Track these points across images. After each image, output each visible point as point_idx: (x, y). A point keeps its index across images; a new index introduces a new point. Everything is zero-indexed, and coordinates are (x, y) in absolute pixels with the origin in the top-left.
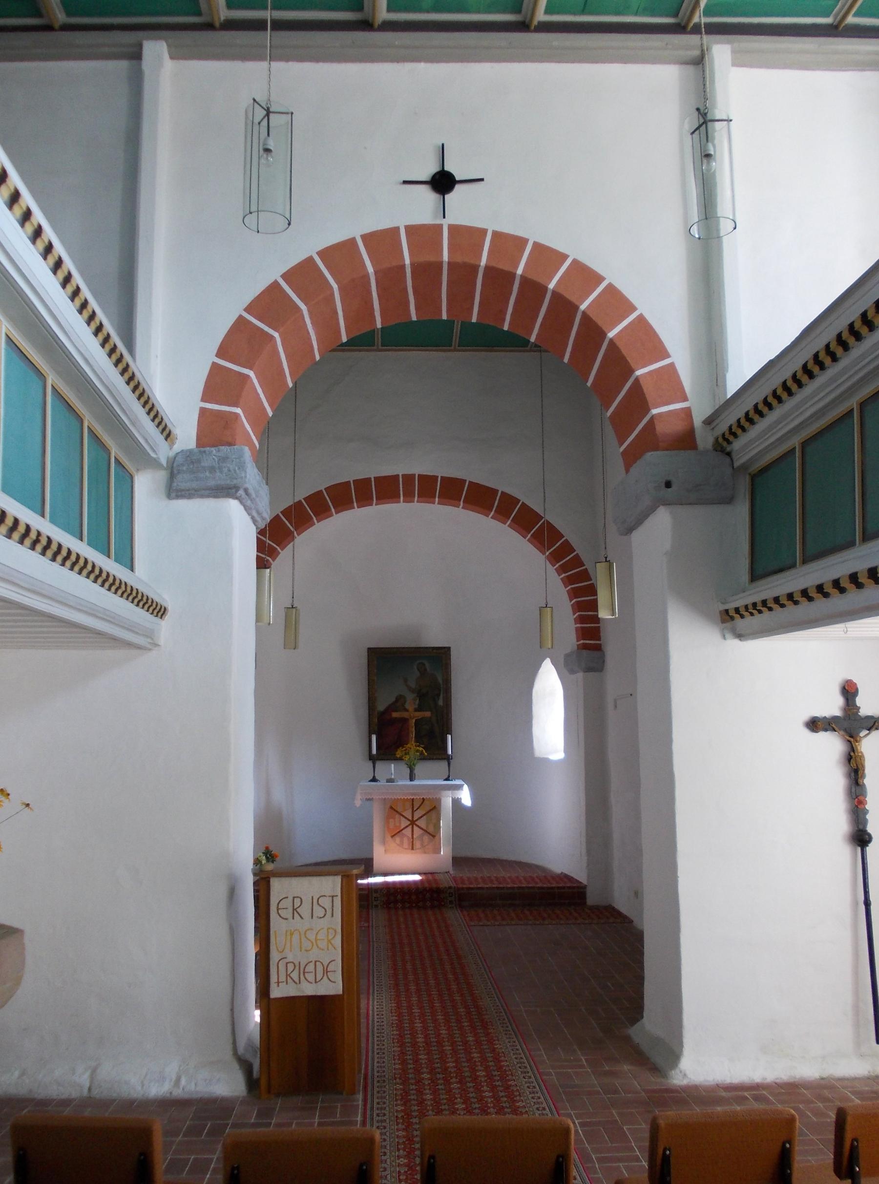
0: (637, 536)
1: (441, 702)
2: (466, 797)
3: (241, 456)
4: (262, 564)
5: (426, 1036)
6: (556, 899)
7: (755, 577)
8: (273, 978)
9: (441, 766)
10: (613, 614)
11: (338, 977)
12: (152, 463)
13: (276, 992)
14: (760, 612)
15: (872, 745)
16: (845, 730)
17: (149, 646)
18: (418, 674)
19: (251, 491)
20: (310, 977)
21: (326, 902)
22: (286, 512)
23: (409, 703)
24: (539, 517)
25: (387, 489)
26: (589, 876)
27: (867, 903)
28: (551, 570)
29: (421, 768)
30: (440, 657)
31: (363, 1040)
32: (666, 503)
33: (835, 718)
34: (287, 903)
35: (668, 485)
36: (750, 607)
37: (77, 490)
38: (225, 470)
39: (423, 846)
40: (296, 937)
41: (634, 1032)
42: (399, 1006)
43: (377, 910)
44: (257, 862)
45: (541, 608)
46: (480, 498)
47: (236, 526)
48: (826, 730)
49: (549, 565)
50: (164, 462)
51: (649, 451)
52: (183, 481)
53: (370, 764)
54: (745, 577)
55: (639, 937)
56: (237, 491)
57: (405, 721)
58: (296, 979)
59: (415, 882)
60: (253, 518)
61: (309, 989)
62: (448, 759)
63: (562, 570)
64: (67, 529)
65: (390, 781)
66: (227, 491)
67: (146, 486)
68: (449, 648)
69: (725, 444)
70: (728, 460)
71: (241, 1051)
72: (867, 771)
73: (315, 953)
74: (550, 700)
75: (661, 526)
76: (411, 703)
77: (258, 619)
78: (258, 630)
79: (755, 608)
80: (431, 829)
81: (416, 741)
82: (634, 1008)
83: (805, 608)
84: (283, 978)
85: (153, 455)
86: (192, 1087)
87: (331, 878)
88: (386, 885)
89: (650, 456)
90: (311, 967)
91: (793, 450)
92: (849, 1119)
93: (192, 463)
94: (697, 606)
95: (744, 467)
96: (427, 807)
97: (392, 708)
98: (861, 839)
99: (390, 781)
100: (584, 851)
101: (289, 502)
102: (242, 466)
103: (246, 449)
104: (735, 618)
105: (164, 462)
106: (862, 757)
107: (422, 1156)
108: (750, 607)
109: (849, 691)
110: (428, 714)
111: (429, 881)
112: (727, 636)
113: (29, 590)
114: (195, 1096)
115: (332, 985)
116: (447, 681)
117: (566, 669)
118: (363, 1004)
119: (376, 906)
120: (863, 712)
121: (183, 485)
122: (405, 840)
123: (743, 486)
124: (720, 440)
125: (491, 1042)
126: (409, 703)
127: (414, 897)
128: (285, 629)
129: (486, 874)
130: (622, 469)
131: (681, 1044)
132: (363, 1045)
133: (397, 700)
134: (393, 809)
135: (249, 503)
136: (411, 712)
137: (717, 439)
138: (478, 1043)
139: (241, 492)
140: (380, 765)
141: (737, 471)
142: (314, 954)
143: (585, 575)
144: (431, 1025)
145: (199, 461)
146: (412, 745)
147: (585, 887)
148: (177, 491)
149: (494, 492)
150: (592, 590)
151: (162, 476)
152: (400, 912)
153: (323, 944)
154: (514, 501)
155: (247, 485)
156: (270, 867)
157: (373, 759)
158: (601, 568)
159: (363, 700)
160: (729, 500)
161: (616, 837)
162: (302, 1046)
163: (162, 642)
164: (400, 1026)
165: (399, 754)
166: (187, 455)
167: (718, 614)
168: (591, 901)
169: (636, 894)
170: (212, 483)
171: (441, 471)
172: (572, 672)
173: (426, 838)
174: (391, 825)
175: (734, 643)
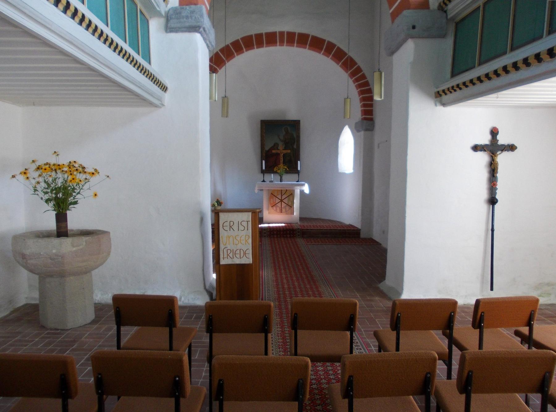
0: (396, 56)
1: (295, 147)
2: (306, 189)
3: (201, 10)
4: (213, 70)
5: (288, 285)
6: (347, 235)
7: (454, 74)
8: (221, 256)
9: (295, 176)
10: (381, 97)
11: (250, 256)
12: (158, 14)
13: (223, 262)
14: (455, 91)
15: (502, 158)
16: (490, 151)
17: (160, 105)
18: (284, 133)
19: (206, 29)
20: (238, 256)
21: (245, 224)
22: (222, 50)
23: (280, 146)
24: (345, 54)
25: (271, 39)
26: (362, 226)
27: (493, 230)
28: (351, 81)
29: (285, 177)
30: (295, 125)
31: (261, 286)
32: (412, 37)
33: (486, 145)
34: (227, 224)
35: (414, 27)
36: (450, 88)
37: (123, 22)
38: (194, 18)
39: (286, 211)
40: (231, 239)
41: (381, 286)
42: (276, 274)
43: (266, 237)
44: (213, 205)
45: (345, 99)
46: (317, 44)
47: (198, 48)
48: (481, 151)
49: (350, 79)
50: (163, 13)
51: (405, 9)
52: (172, 24)
53: (262, 175)
54: (449, 75)
55: (385, 251)
56: (200, 29)
57: (278, 154)
58: (232, 257)
59: (282, 226)
60: (207, 45)
61: (237, 261)
62: (298, 172)
63: (356, 81)
64: (119, 36)
65: (271, 181)
66: (194, 29)
67: (155, 26)
68: (299, 121)
69: (444, 6)
70: (445, 15)
71: (207, 287)
72: (499, 170)
73: (239, 247)
74: (347, 142)
75: (409, 47)
76: (281, 147)
77: (211, 98)
78: (211, 103)
79: (453, 89)
80: (290, 204)
81: (283, 164)
82: (382, 276)
83: (479, 87)
84: (225, 256)
85: (158, 9)
86: (186, 301)
87: (246, 213)
88: (269, 227)
89: (406, 12)
90: (238, 252)
91: (479, 7)
92: (481, 303)
93: (177, 14)
94: (424, 89)
95: (453, 19)
96: (288, 194)
97: (272, 148)
98: (492, 201)
99: (271, 181)
100: (360, 214)
101: (222, 45)
102: (202, 16)
103: (204, 7)
104: (442, 96)
105: (163, 13)
106: (497, 164)
107: (291, 314)
108: (450, 88)
109: (494, 133)
110: (289, 151)
111: (288, 226)
112: (438, 104)
113: (104, 64)
114: (188, 305)
115: (248, 260)
116: (298, 137)
117: (356, 130)
118: (261, 272)
119: (265, 236)
120: (500, 143)
121: (173, 26)
122: (278, 208)
123: (452, 29)
124: (442, 4)
125: (317, 288)
126: (280, 146)
127: (282, 233)
128: (222, 106)
129: (315, 224)
130: (390, 21)
131: (402, 289)
132: (261, 288)
133: (274, 145)
134: (272, 194)
135: (205, 36)
136: (281, 150)
137: (440, 4)
138: (311, 288)
139: (201, 29)
140: (266, 175)
141: (448, 21)
142: (239, 246)
143: (367, 84)
144: (290, 281)
145: (180, 13)
146: (281, 165)
147: (360, 230)
148: (170, 29)
149: (324, 41)
150: (370, 91)
151: (162, 21)
152: (276, 239)
153: (243, 242)
154: (333, 45)
155: (204, 26)
156: (219, 208)
157: (263, 172)
158: (376, 74)
159: (258, 145)
160: (443, 36)
161: (375, 210)
162: (234, 281)
163: (166, 104)
164: (277, 281)
165: (275, 169)
166: (175, 10)
167: (434, 95)
168: (362, 236)
169: (384, 232)
170: (187, 24)
171: (298, 29)
172: (358, 131)
173: (288, 208)
174: (272, 202)
175: (440, 108)
